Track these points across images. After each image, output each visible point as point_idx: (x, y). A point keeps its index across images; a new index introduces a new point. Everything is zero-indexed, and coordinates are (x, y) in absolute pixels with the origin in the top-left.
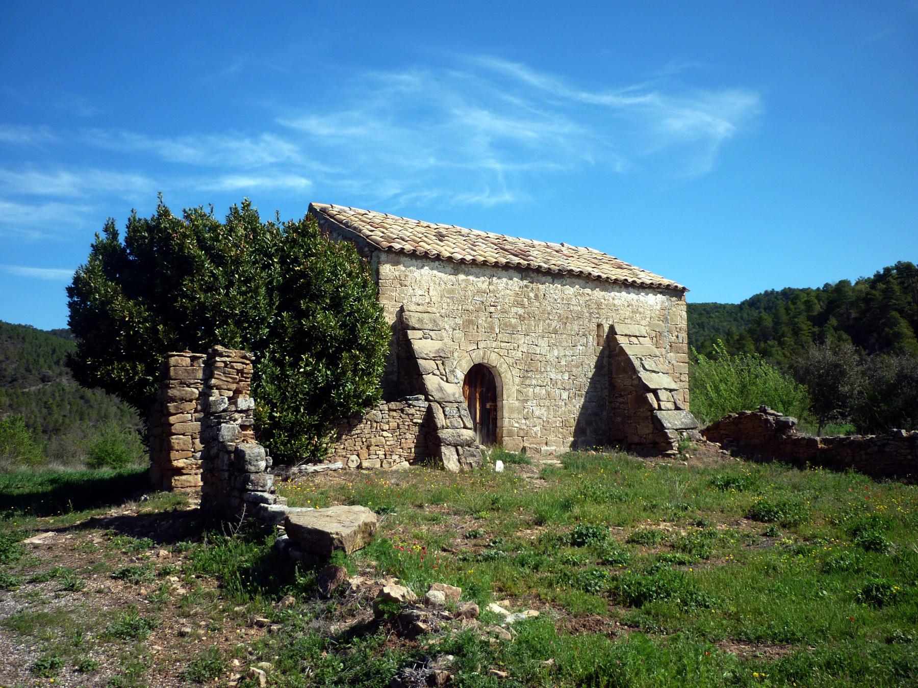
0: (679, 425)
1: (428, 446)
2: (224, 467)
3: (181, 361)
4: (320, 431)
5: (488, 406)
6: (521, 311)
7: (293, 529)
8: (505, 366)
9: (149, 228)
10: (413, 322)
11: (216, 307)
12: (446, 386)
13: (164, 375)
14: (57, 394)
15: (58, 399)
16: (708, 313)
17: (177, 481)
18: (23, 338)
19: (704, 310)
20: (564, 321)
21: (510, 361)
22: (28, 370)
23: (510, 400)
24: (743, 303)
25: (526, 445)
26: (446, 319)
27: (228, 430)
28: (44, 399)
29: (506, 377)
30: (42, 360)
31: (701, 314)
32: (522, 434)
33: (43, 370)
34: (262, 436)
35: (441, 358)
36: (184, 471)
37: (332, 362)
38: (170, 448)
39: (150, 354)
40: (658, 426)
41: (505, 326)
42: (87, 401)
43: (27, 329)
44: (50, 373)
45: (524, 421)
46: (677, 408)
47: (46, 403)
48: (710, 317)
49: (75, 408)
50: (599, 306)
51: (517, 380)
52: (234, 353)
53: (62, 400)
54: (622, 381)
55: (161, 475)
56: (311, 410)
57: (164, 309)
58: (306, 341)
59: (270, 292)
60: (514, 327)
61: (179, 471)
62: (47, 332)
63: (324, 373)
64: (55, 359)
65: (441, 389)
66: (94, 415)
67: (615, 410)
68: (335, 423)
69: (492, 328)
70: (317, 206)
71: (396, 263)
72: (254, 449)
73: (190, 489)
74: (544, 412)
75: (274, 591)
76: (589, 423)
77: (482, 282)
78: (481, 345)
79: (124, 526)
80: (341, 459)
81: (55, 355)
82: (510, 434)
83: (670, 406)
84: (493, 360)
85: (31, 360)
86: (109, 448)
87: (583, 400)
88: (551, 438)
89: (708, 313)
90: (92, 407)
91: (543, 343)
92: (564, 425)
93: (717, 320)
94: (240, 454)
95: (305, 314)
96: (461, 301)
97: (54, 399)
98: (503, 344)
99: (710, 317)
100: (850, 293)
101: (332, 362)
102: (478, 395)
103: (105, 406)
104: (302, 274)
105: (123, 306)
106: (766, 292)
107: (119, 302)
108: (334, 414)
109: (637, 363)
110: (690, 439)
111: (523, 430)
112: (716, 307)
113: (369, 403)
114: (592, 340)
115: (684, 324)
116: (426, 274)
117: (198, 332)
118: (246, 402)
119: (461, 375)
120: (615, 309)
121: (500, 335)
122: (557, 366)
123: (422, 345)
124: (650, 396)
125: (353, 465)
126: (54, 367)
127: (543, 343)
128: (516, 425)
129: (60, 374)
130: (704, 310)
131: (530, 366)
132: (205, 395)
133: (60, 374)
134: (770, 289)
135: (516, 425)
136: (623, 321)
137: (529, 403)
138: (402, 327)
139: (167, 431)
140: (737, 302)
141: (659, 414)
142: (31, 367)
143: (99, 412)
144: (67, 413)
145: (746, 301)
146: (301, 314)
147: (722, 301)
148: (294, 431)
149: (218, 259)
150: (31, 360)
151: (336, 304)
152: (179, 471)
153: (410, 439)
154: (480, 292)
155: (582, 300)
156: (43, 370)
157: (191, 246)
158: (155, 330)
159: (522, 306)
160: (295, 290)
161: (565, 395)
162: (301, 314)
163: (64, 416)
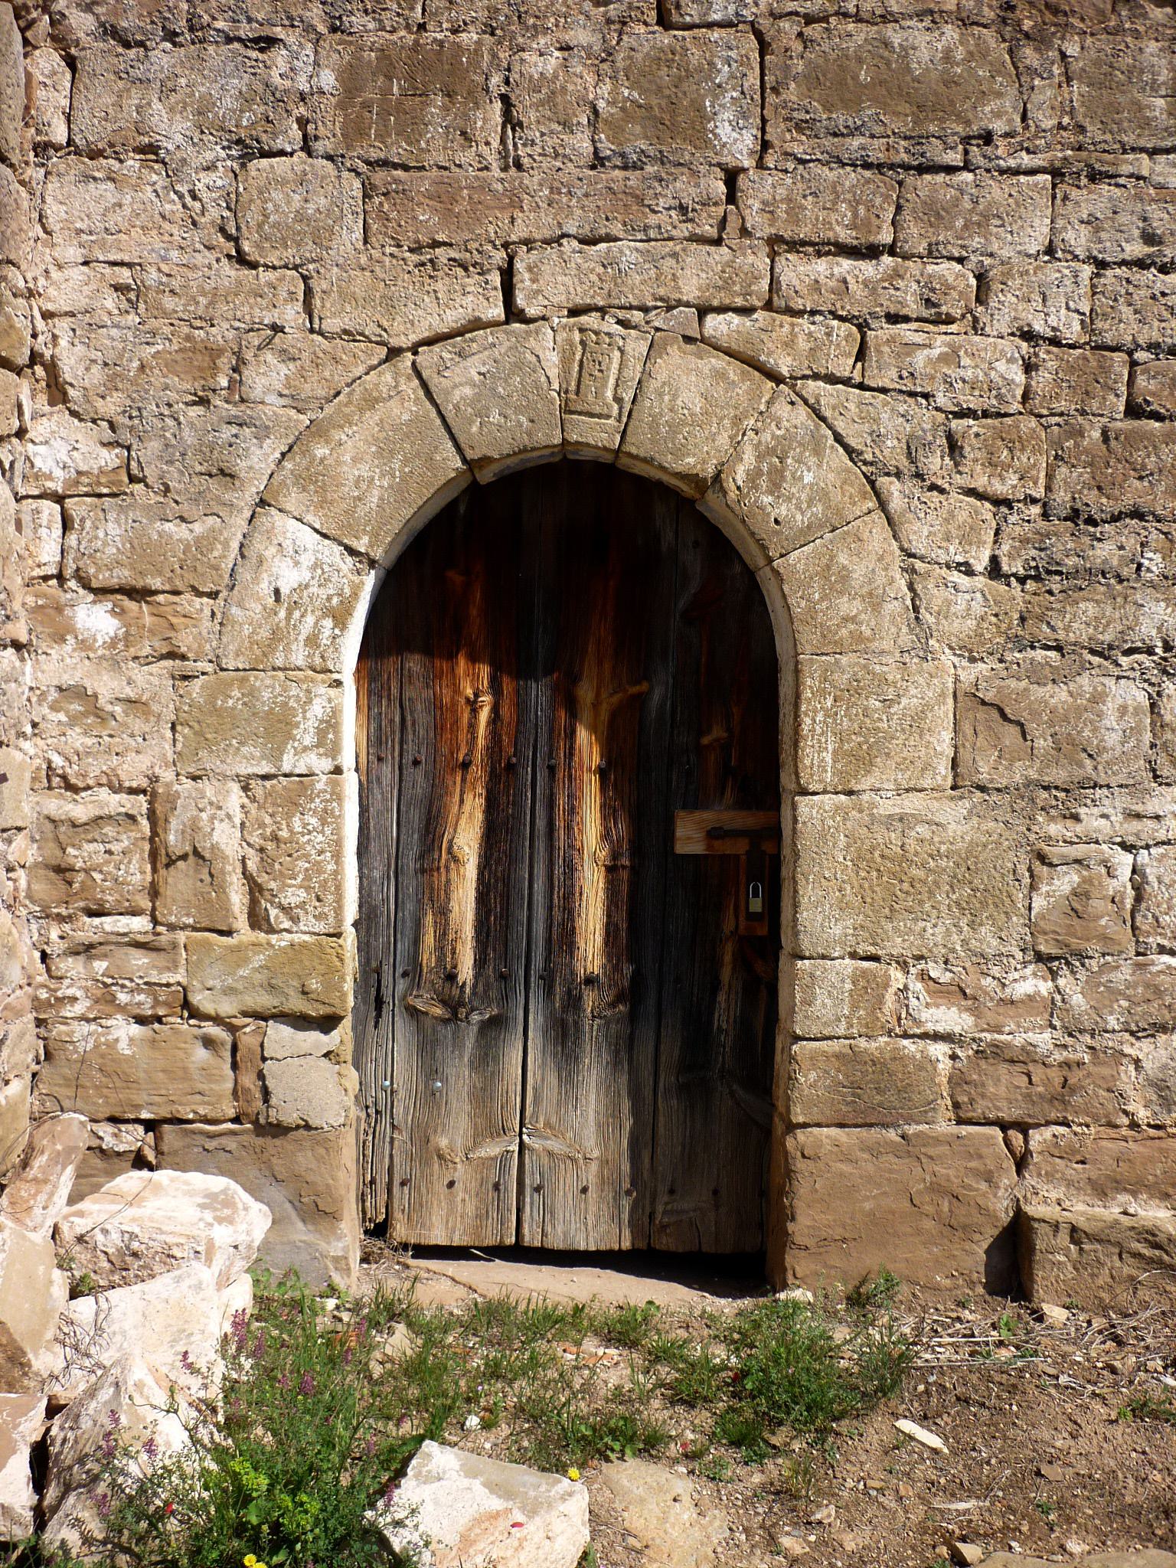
5: (689, 836)
8: (821, 473)
21: (892, 424)
25: (1050, 1201)
26: (163, 58)
29: (837, 581)
32: (1002, 1093)
36: (859, 364)
45: (1031, 983)
51: (964, 604)
60: (932, 100)
78: (549, 283)
87: (713, 1251)
98: (796, 271)
102: (588, 746)
111: (1023, 1059)
121: (758, 189)
128: (950, 1018)
135: (950, 1018)
137: (1100, 818)
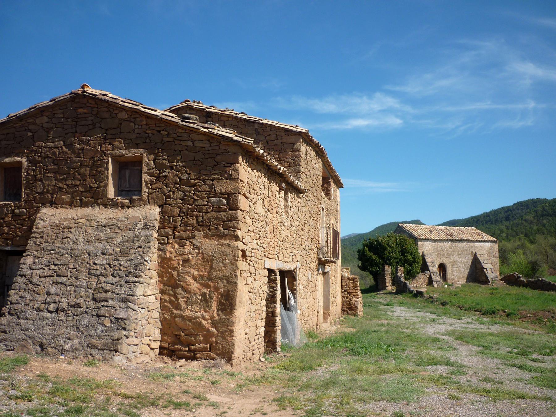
0: (492, 277)
1: (430, 282)
10: (426, 255)
12: (434, 269)
13: (384, 270)
20: (463, 251)
23: (449, 271)
35: (432, 263)
38: (385, 282)
40: (487, 277)
41: (447, 254)
54: (478, 266)
55: (385, 287)
57: (381, 257)
67: (477, 274)
74: (458, 274)
77: (441, 244)
84: (445, 262)
88: (460, 280)
91: (457, 257)
92: (463, 277)
101: (411, 265)
107: (373, 256)
109: (482, 262)
113: (418, 273)
114: (470, 256)
116: (428, 243)
117: (387, 261)
119: (437, 266)
120: (477, 247)
123: (428, 260)
124: (485, 270)
127: (457, 257)
138: (423, 256)
141: (487, 274)
149: (390, 247)
153: (426, 281)
154: (441, 246)
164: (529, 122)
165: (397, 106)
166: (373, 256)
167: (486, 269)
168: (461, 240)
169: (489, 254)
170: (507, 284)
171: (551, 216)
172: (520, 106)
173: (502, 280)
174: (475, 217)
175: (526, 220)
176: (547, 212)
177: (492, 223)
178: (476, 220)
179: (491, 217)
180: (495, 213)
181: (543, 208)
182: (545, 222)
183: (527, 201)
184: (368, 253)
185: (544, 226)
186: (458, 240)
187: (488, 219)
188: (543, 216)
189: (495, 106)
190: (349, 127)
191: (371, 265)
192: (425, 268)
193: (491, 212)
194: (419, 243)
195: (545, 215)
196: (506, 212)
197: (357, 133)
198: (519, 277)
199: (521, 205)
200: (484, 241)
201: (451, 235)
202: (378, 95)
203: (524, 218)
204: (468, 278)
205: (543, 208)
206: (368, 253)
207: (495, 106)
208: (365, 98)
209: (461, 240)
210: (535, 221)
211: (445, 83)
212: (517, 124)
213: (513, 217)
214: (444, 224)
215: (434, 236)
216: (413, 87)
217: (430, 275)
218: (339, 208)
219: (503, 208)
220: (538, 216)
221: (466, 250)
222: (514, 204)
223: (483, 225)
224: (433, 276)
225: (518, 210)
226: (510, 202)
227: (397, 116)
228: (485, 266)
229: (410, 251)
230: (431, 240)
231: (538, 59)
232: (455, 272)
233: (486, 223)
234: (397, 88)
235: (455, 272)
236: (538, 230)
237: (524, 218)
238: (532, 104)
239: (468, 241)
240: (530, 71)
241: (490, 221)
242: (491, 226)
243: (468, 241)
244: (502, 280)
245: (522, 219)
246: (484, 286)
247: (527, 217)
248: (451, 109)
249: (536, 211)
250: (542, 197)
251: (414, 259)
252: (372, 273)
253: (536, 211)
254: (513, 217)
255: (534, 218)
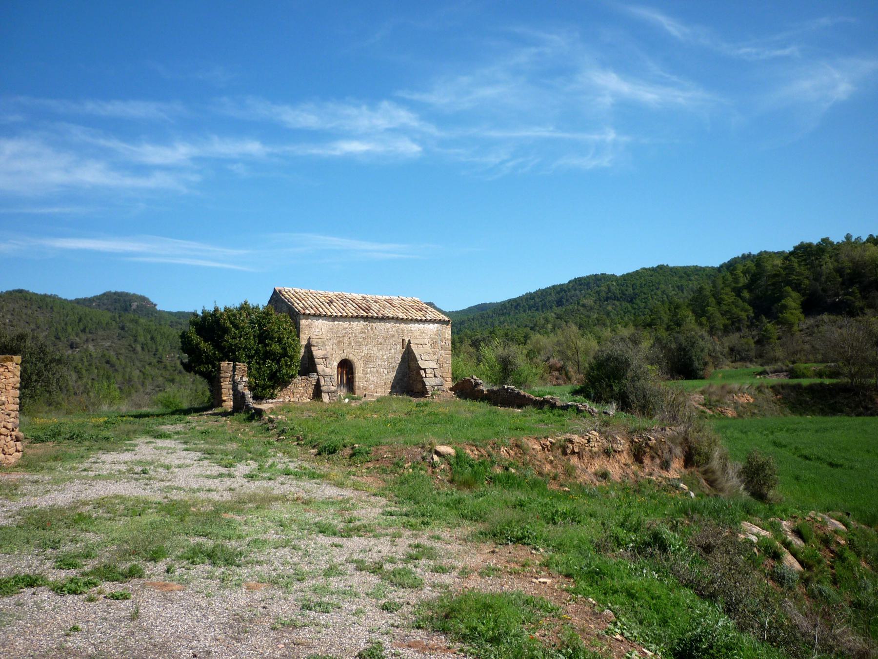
0: (433, 384)
1: (317, 393)
2: (239, 398)
3: (224, 364)
4: (274, 388)
6: (364, 336)
7: (255, 409)
9: (212, 315)
10: (314, 343)
11: (236, 345)
12: (328, 369)
13: (219, 369)
14: (85, 360)
15: (86, 363)
16: (688, 276)
17: (224, 404)
18: (51, 308)
19: (685, 273)
20: (385, 339)
22: (58, 338)
23: (358, 374)
24: (721, 266)
27: (240, 387)
28: (74, 364)
30: (70, 329)
31: (681, 277)
33: (72, 337)
34: (251, 389)
35: (325, 358)
37: (278, 362)
38: (221, 394)
39: (215, 362)
40: (424, 384)
41: (356, 342)
42: (113, 366)
43: (54, 298)
44: (78, 339)
46: (435, 376)
47: (75, 368)
48: (690, 280)
49: (102, 372)
50: (403, 331)
52: (242, 364)
53: (90, 365)
54: (412, 364)
55: (220, 402)
56: (270, 379)
57: (217, 346)
58: (268, 355)
59: (254, 336)
60: (361, 343)
61: (225, 401)
62: (71, 301)
63: (275, 366)
64: (82, 327)
65: (324, 371)
66: (119, 378)
67: (408, 379)
68: (279, 385)
69: (350, 343)
70: (277, 289)
71: (307, 319)
72: (247, 392)
73: (229, 405)
74: (376, 378)
75: (251, 421)
76: (398, 383)
77: (346, 324)
79: (214, 414)
80: (283, 397)
81: (81, 324)
82: (359, 388)
83: (432, 375)
84: (351, 357)
85: (60, 328)
86: (171, 399)
88: (379, 390)
89: (688, 276)
90: (116, 370)
91: (375, 349)
92: (386, 384)
93: (695, 283)
94: (243, 393)
95: (268, 345)
96: (336, 333)
97: (83, 364)
99: (690, 280)
100: (769, 268)
101: (278, 362)
103: (128, 370)
104: (266, 331)
105: (204, 345)
106: (743, 255)
107: (202, 344)
108: (279, 381)
109: (418, 357)
110: (438, 390)
112: (697, 270)
113: (293, 376)
114: (399, 347)
115: (450, 337)
116: (320, 322)
117: (231, 354)
118: (245, 379)
119: (335, 364)
120: (412, 332)
122: (382, 359)
123: (317, 353)
124: (422, 372)
125: (287, 400)
126: (81, 335)
127: (375, 349)
129: (87, 341)
130: (685, 273)
131: (368, 359)
132: (234, 375)
133: (87, 341)
134: (747, 253)
136: (416, 337)
138: (309, 346)
139: (220, 388)
140: (717, 265)
141: (425, 379)
142: (60, 334)
143: (124, 375)
144: (94, 376)
145: (725, 264)
146: (266, 345)
147: (702, 263)
148: (264, 388)
149: (236, 326)
150: (60, 328)
151: (280, 341)
152: (225, 401)
153: (310, 391)
154: (345, 329)
155: (394, 329)
156: (72, 337)
157: (228, 324)
158: (215, 353)
159: (365, 333)
160: (263, 337)
161: (386, 371)
162: (266, 345)
163: (93, 379)
164: (605, 162)
165: (415, 124)
166: (202, 344)
167: (424, 369)
168: (384, 319)
169: (434, 344)
170: (459, 396)
171: (618, 300)
172: (595, 137)
173: (451, 389)
174: (514, 300)
175: (584, 306)
176: (614, 293)
177: (537, 310)
178: (515, 304)
179: (537, 300)
180: (543, 294)
181: (609, 288)
182: (609, 308)
183: (588, 277)
184: (196, 339)
185: (608, 314)
186: (377, 318)
187: (532, 302)
188: (607, 299)
189: (559, 135)
190: (337, 153)
191: (200, 362)
192: (309, 366)
193: (536, 293)
194: (303, 322)
195: (611, 298)
196: (558, 293)
197: (349, 163)
198: (477, 384)
199: (580, 283)
200: (426, 321)
201: (368, 309)
202: (385, 104)
203: (581, 303)
204: (393, 387)
205: (609, 288)
206: (196, 339)
207: (559, 135)
208: (364, 108)
209: (384, 319)
210: (597, 307)
211: (489, 92)
212: (588, 163)
213: (567, 300)
214: (427, 304)
215: (333, 311)
216: (440, 97)
217: (318, 381)
218: (357, 296)
219: (554, 287)
220: (600, 300)
221: (393, 336)
222: (570, 282)
223: (524, 311)
224: (322, 382)
225: (575, 290)
226: (564, 279)
227: (414, 140)
228: (422, 364)
229: (276, 335)
230: (326, 317)
231: (624, 67)
232: (369, 376)
233: (530, 309)
234: (416, 96)
235: (369, 376)
236: (598, 320)
237: (581, 303)
238: (611, 135)
239: (397, 320)
240: (610, 84)
241: (534, 305)
242: (536, 313)
243: (397, 320)
244: (451, 389)
245: (578, 303)
246: (415, 400)
247: (586, 301)
248: (495, 134)
249: (598, 293)
250: (609, 272)
251: (284, 349)
252: (202, 374)
253: (598, 293)
254: (567, 300)
255: (595, 302)
